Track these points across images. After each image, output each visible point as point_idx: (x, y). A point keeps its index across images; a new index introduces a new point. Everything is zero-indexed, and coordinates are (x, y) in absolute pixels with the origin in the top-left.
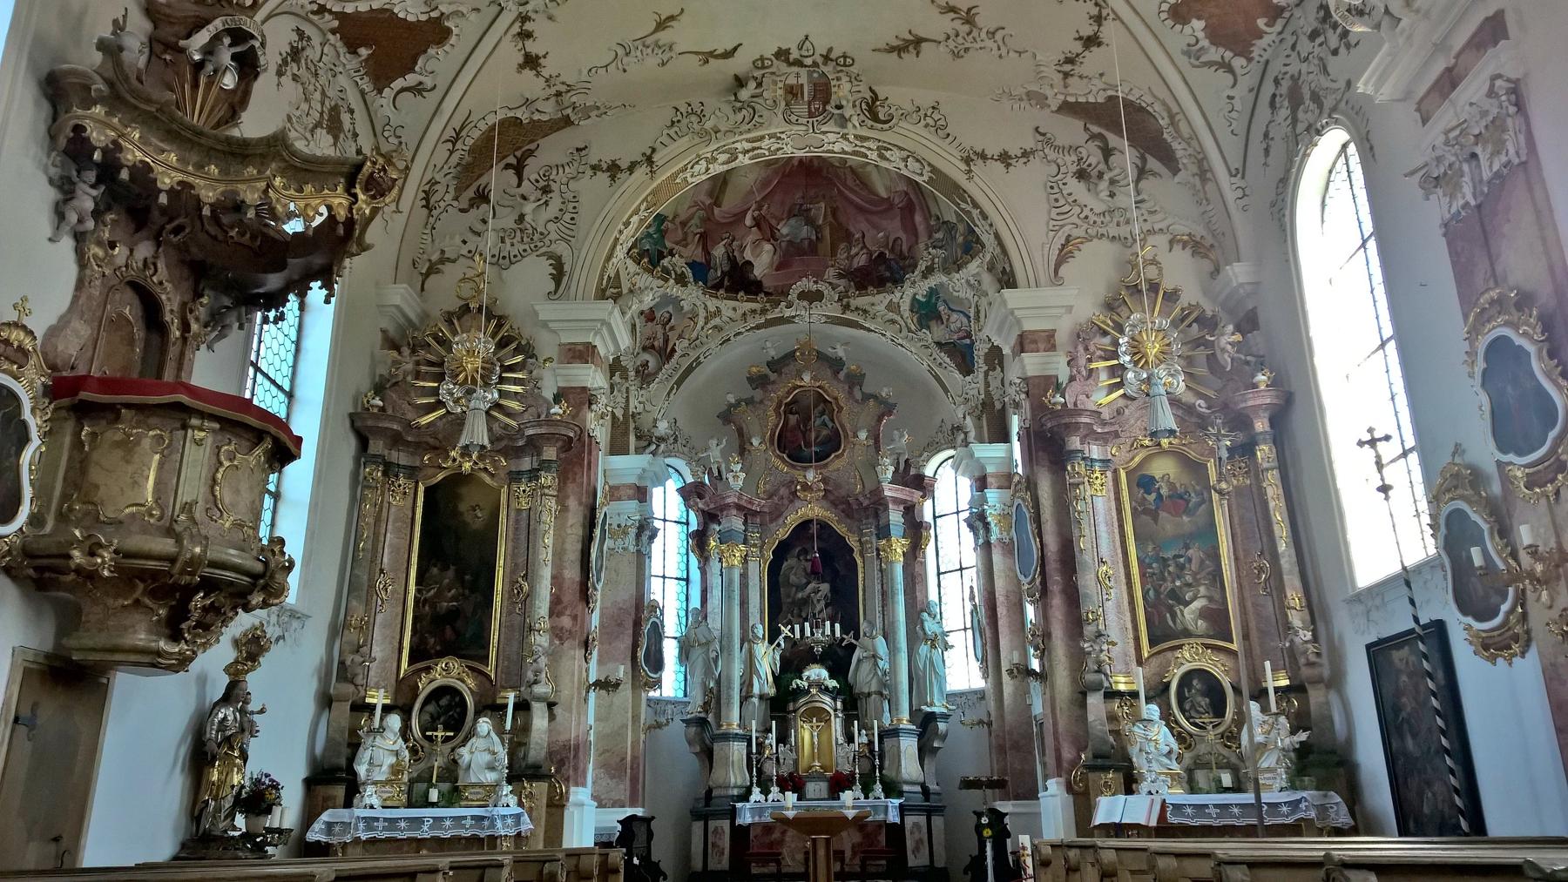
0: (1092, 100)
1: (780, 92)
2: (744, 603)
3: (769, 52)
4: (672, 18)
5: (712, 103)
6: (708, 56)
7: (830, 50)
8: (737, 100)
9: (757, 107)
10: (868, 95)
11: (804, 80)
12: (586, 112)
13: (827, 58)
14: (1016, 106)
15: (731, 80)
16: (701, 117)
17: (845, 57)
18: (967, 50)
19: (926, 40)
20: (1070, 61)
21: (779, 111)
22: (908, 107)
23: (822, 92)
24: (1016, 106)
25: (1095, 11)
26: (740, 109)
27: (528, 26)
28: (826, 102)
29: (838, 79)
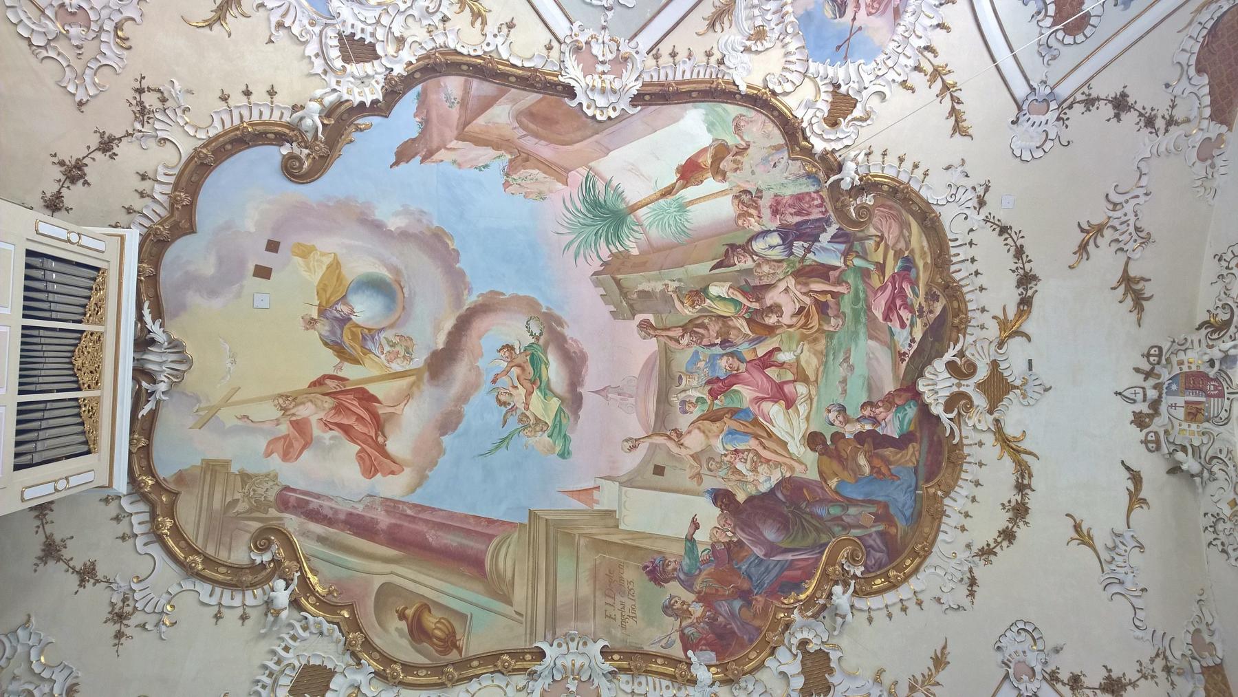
0: (1206, 90)
1: (1194, 426)
2: (62, 330)
3: (1137, 434)
4: (1077, 528)
5: (1206, 505)
6: (1135, 499)
7: (1137, 370)
8: (1200, 475)
9: (1210, 453)
10: (1204, 331)
11: (1180, 400)
12: (1199, 643)
13: (1148, 375)
14: (1222, 170)
15: (1173, 479)
16: (1218, 518)
17: (1148, 355)
18: (1137, 229)
19: (1125, 271)
20: (1150, 122)
21: (1216, 430)
22: (1219, 287)
23: (1194, 381)
24: (1222, 170)
25: (1079, 108)
26: (1211, 472)
27: (1064, 675)
28: (1205, 376)
29: (1181, 363)
